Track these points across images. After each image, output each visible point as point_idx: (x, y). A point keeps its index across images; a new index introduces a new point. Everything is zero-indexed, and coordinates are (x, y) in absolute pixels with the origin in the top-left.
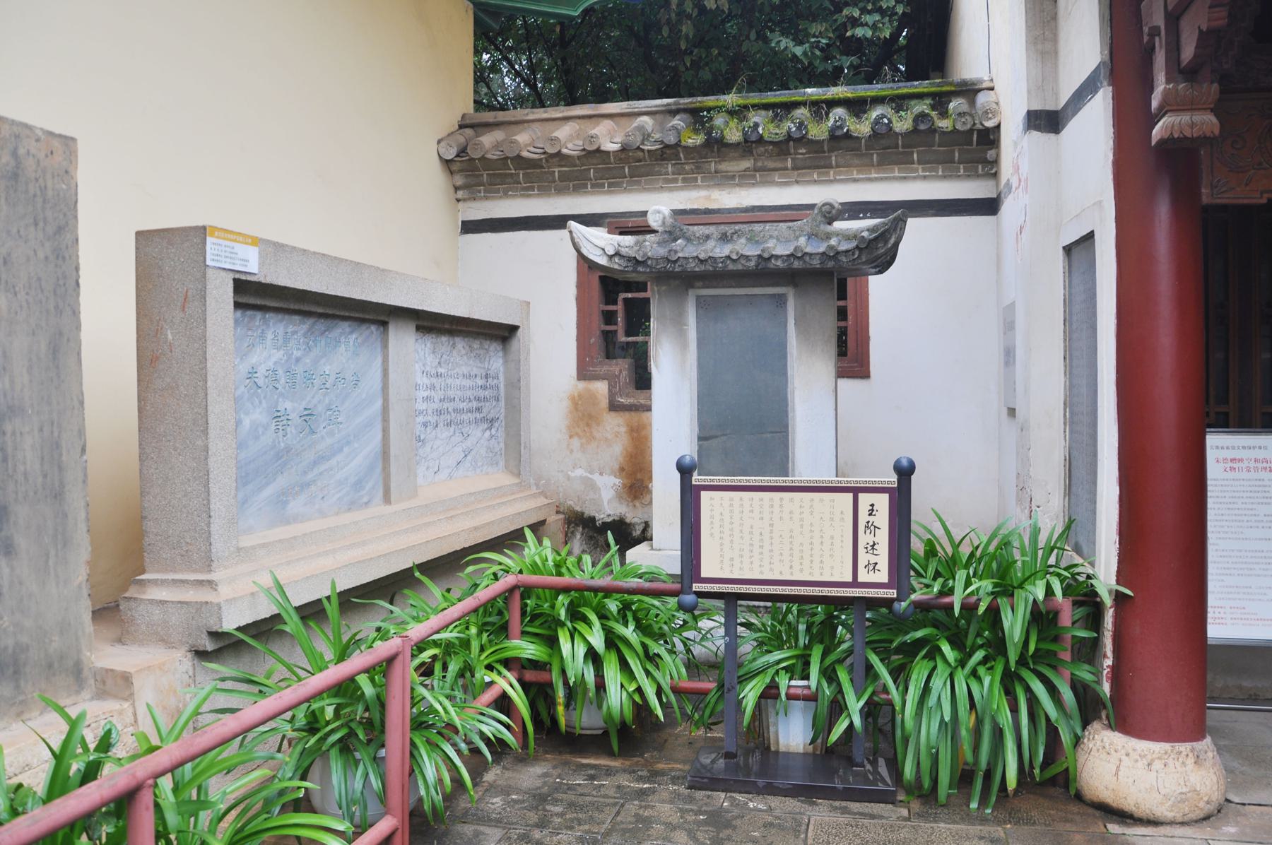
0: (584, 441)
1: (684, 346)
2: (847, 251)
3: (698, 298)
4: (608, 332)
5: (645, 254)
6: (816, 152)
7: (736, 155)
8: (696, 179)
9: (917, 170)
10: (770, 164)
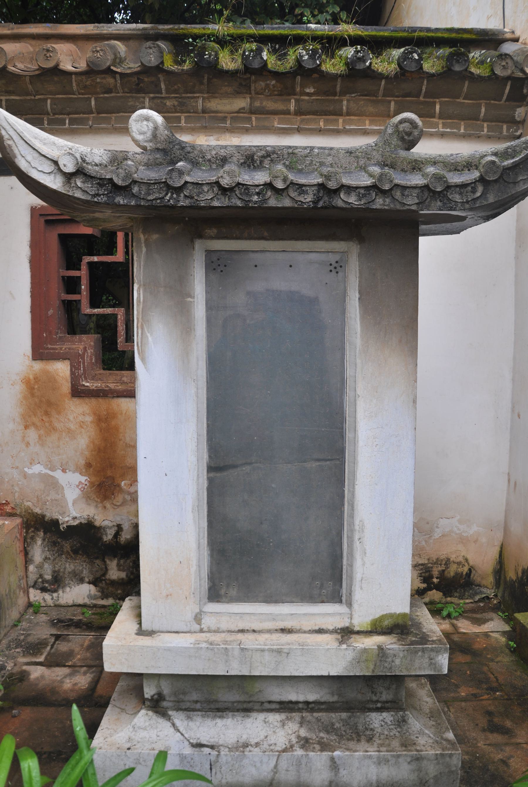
0: (42, 432)
1: (186, 329)
2: (463, 186)
3: (209, 253)
4: (70, 302)
5: (128, 175)
6: (326, 93)
7: (229, 90)
8: (179, 119)
9: (436, 126)
10: (270, 105)
